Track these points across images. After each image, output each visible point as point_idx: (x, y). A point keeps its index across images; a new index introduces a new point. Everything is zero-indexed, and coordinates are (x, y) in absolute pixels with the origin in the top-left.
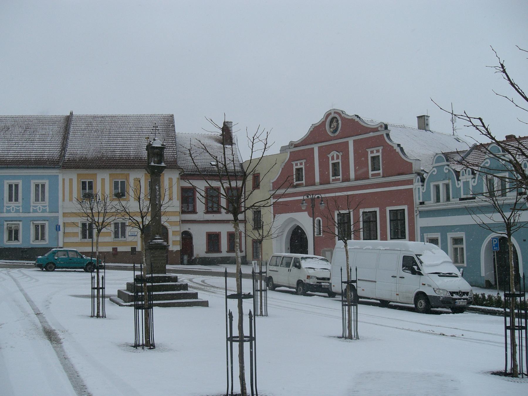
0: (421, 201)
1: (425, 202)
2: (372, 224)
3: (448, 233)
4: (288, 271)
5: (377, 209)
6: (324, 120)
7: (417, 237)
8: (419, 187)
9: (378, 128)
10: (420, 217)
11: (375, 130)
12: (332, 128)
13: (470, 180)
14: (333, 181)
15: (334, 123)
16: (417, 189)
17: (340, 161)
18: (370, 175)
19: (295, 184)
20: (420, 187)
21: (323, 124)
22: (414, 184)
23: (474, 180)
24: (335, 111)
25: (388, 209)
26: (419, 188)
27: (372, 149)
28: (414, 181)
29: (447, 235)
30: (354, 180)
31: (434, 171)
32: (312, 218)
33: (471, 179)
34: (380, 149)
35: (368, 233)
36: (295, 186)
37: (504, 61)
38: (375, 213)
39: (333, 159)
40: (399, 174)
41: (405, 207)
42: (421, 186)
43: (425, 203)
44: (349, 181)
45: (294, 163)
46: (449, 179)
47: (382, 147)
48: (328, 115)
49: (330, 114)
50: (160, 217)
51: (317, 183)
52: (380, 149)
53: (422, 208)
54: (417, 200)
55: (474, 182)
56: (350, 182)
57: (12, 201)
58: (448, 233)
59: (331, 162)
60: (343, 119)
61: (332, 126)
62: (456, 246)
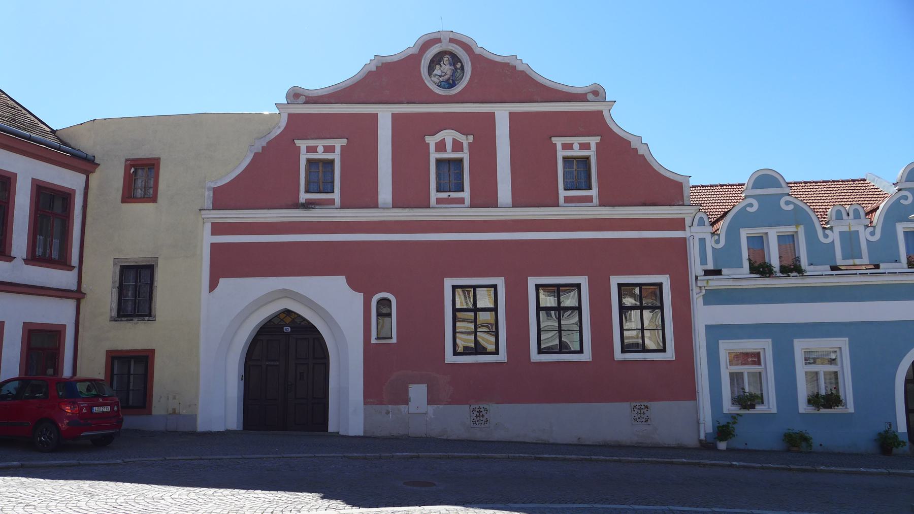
0: (710, 266)
1: (724, 271)
3: (720, 341)
5: (665, 280)
6: (415, 51)
9: (586, 94)
11: (580, 97)
12: (436, 75)
13: (861, 229)
15: (444, 64)
17: (465, 155)
19: (303, 197)
22: (687, 228)
26: (702, 241)
27: (568, 140)
28: (688, 222)
30: (340, 207)
31: (751, 205)
32: (360, 296)
33: (863, 227)
34: (593, 141)
41: (665, 280)
42: (710, 235)
43: (881, 267)
44: (497, 207)
45: (302, 144)
46: (797, 224)
47: (598, 139)
48: (427, 43)
49: (437, 41)
52: (593, 141)
54: (696, 268)
55: (872, 234)
56: (428, 210)
58: (720, 341)
59: (434, 156)
61: (437, 71)
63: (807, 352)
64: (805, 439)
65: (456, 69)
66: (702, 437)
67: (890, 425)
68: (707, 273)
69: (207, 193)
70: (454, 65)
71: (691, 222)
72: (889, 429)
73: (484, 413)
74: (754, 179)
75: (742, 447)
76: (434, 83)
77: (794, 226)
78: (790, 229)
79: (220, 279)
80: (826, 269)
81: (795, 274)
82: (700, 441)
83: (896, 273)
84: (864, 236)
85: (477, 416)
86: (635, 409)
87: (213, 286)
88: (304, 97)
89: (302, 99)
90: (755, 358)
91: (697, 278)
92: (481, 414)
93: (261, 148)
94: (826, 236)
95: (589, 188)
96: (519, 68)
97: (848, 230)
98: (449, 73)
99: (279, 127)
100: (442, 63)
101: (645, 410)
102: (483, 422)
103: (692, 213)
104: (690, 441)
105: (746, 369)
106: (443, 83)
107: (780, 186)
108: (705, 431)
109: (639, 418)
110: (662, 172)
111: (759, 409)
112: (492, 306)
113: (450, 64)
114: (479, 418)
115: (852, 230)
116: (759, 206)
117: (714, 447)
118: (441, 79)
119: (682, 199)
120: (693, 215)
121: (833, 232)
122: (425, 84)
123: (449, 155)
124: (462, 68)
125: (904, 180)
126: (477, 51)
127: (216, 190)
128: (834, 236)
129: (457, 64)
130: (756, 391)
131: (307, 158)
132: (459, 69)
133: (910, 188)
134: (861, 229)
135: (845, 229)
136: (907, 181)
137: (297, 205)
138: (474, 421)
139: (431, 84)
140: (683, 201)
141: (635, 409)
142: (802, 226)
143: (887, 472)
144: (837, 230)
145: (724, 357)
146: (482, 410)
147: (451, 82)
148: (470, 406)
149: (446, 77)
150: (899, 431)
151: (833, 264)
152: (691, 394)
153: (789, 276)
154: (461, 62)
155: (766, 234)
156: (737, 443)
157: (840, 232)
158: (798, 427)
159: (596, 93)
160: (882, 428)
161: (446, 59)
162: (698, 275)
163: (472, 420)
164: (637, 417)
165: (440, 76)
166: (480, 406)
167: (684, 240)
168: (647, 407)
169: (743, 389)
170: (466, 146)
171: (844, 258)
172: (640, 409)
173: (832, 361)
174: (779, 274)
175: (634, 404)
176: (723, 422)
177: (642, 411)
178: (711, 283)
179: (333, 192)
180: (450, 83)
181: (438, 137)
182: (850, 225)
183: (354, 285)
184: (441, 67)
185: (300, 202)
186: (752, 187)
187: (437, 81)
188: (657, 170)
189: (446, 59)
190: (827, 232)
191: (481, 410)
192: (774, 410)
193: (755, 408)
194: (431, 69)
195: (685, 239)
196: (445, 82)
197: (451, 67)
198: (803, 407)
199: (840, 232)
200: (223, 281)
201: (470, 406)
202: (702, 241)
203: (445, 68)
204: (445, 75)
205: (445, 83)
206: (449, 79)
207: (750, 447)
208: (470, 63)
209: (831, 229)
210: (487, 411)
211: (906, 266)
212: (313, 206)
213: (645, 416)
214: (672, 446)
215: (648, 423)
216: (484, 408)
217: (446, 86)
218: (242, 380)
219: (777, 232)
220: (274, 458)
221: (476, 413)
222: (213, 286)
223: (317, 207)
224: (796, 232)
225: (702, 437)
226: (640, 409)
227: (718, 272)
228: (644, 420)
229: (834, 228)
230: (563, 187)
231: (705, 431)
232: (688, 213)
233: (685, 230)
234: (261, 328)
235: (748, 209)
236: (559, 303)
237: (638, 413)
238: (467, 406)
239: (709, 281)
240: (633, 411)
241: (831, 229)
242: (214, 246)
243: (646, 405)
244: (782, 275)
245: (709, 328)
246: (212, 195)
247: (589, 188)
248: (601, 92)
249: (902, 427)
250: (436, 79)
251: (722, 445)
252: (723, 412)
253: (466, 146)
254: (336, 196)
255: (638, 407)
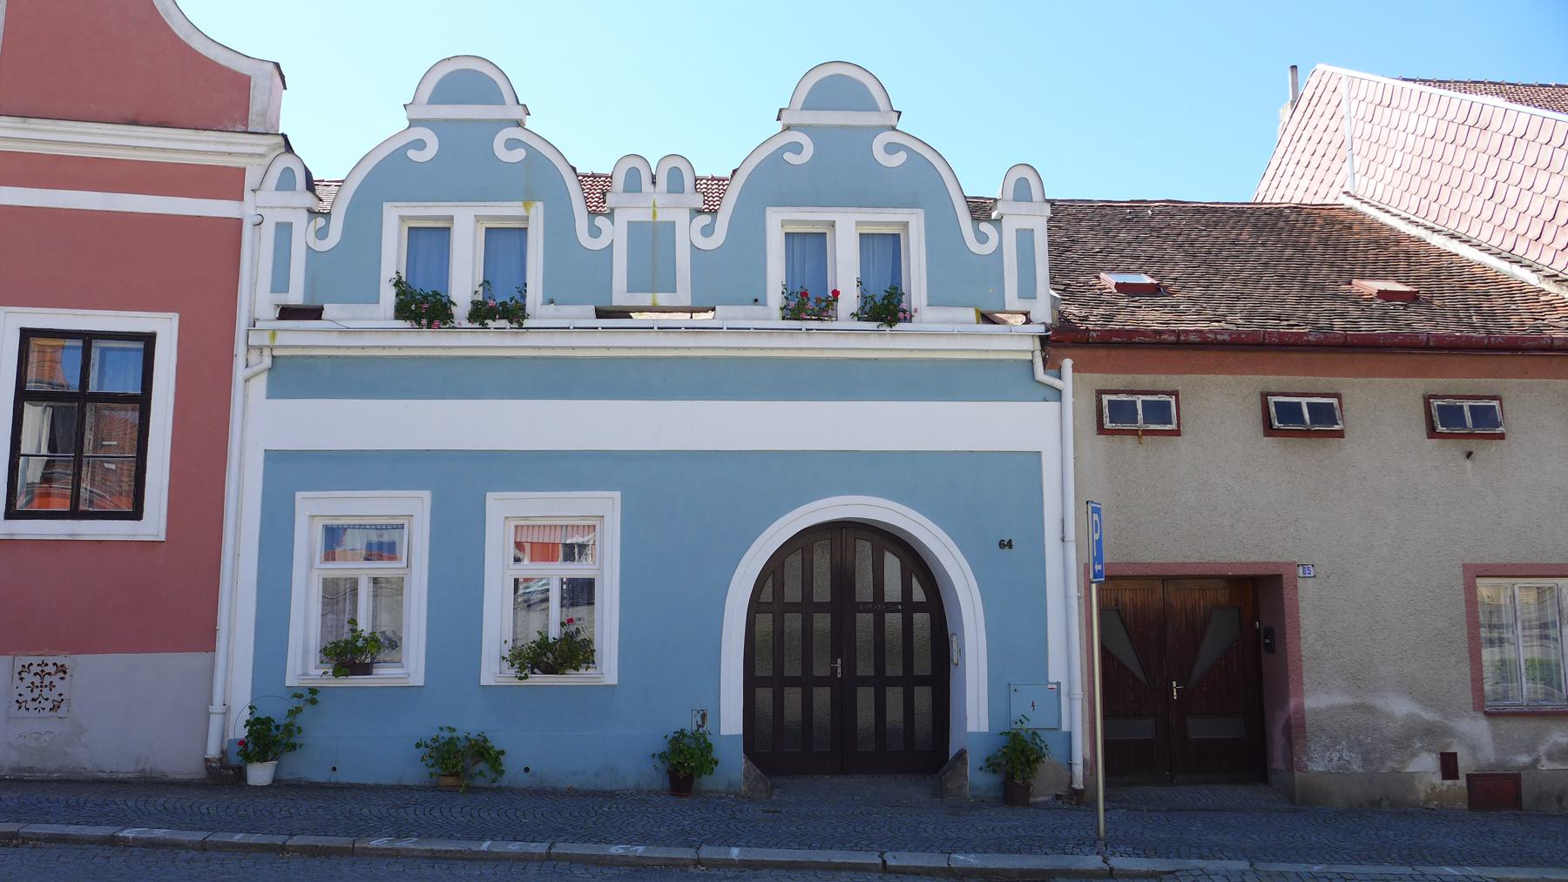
1: (330, 310)
3: (299, 495)
4: (1502, 436)
5: (165, 327)
8: (285, 217)
13: (681, 218)
16: (268, 231)
20: (300, 221)
22: (248, 195)
23: (705, 220)
26: (284, 231)
28: (250, 180)
33: (686, 214)
37: (1294, 68)
38: (140, 345)
41: (165, 327)
46: (528, 199)
53: (299, 337)
55: (707, 231)
58: (299, 495)
64: (482, 751)
67: (704, 717)
68: (287, 313)
71: (259, 180)
72: (699, 726)
74: (437, 80)
75: (320, 776)
77: (521, 203)
78: (509, 210)
80: (584, 314)
81: (504, 323)
83: (597, 328)
84: (688, 234)
86: (23, 675)
94: (595, 232)
97: (651, 219)
101: (55, 679)
103: (261, 155)
104: (181, 761)
109: (34, 700)
110: (197, 44)
111: (384, 675)
112: (134, 388)
115: (658, 219)
117: (241, 775)
119: (245, 118)
120: (267, 161)
121: (613, 224)
125: (799, 102)
128: (615, 234)
130: (385, 625)
133: (810, 126)
134: (681, 218)
135: (643, 216)
136: (807, 106)
140: (246, 125)
141: (23, 675)
142: (540, 205)
143: (1418, 868)
144: (622, 218)
145: (307, 538)
150: (723, 732)
151: (603, 304)
152: (204, 637)
153: (484, 326)
155: (832, 224)
156: (304, 766)
157: (631, 225)
158: (469, 724)
160: (689, 724)
167: (234, 227)
168: (62, 670)
169: (353, 622)
171: (632, 288)
172: (42, 674)
173: (572, 552)
174: (466, 324)
175: (26, 660)
176: (277, 711)
177: (47, 680)
178: (282, 339)
182: (654, 206)
186: (429, 100)
188: (181, 37)
190: (600, 221)
192: (418, 679)
193: (371, 674)
195: (239, 222)
198: (493, 671)
199: (631, 225)
207: (344, 777)
209: (610, 215)
211: (778, 314)
213: (53, 695)
214: (121, 776)
215: (61, 712)
219: (858, 223)
225: (213, 751)
226: (42, 674)
227: (314, 313)
228: (49, 705)
229: (616, 212)
232: (251, 155)
233: (242, 199)
235: (789, 157)
237: (32, 687)
239: (278, 333)
241: (610, 215)
244: (470, 325)
245: (276, 460)
249: (731, 720)
251: (260, 774)
255: (35, 669)
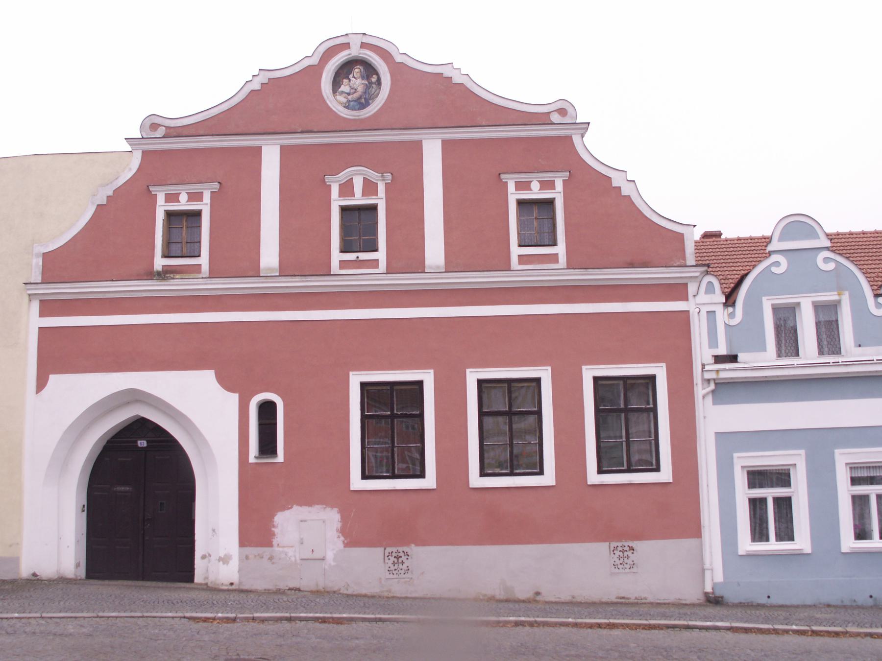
0: (722, 351)
1: (741, 357)
2: (520, 424)
5: (660, 372)
6: (315, 61)
7: (773, 466)
9: (548, 114)
10: (714, 403)
11: (542, 119)
12: (343, 92)
14: (341, 268)
15: (354, 77)
17: (381, 202)
18: (514, 260)
19: (159, 262)
20: (719, 310)
21: (311, 73)
24: (366, 40)
25: (589, 373)
26: (711, 314)
29: (732, 458)
32: (235, 397)
35: (383, 450)
36: (159, 273)
38: (534, 384)
39: (347, 189)
40: (631, 265)
42: (721, 306)
43: (739, 360)
49: (347, 46)
50: (511, 388)
51: (271, 269)
53: (728, 371)
57: (767, 540)
59: (337, 202)
60: (400, 70)
61: (344, 88)
62: (758, 493)
63: (854, 467)
65: (371, 83)
66: (708, 589)
69: (34, 261)
70: (368, 77)
73: (404, 558)
76: (340, 103)
79: (50, 376)
82: (706, 594)
85: (394, 563)
87: (41, 384)
88: (164, 128)
89: (161, 132)
90: (782, 477)
91: (703, 366)
92: (400, 560)
93: (105, 199)
95: (554, 244)
96: (457, 79)
98: (360, 89)
99: (130, 169)
100: (351, 76)
102: (403, 572)
105: (770, 493)
106: (352, 103)
107: (815, 236)
108: (713, 580)
109: (621, 564)
113: (363, 78)
114: (396, 565)
116: (788, 266)
118: (350, 97)
122: (327, 104)
123: (358, 199)
124: (379, 82)
126: (399, 59)
127: (47, 257)
129: (372, 77)
131: (165, 210)
132: (375, 83)
137: (151, 275)
138: (390, 569)
139: (336, 104)
141: (615, 552)
146: (401, 554)
147: (363, 101)
148: (385, 549)
149: (356, 95)
154: (377, 74)
159: (562, 112)
161: (357, 70)
162: (705, 363)
163: (388, 568)
164: (618, 562)
165: (349, 94)
166: (398, 548)
168: (632, 549)
170: (381, 188)
175: (614, 544)
179: (376, 250)
180: (362, 103)
181: (343, 176)
183: (226, 382)
184: (350, 81)
185: (155, 270)
187: (345, 100)
189: (357, 70)
191: (400, 555)
194: (336, 84)
196: (355, 101)
197: (363, 82)
200: (53, 378)
201: (385, 549)
202: (711, 314)
203: (356, 82)
204: (355, 92)
205: (355, 103)
206: (360, 98)
208: (388, 75)
210: (408, 556)
212: (172, 276)
213: (629, 561)
216: (403, 552)
217: (357, 107)
218: (83, 511)
220: (173, 618)
221: (392, 559)
222: (41, 384)
223: (178, 276)
224: (839, 302)
226: (623, 551)
227: (733, 359)
230: (517, 242)
231: (713, 580)
234: (108, 442)
235: (774, 270)
236: (510, 406)
238: (381, 550)
240: (612, 555)
242: (43, 331)
243: (393, 565)
246: (41, 263)
247: (554, 244)
248: (570, 110)
250: (342, 99)
252: (737, 552)
253: (381, 188)
254: (204, 260)
255: (619, 549)
